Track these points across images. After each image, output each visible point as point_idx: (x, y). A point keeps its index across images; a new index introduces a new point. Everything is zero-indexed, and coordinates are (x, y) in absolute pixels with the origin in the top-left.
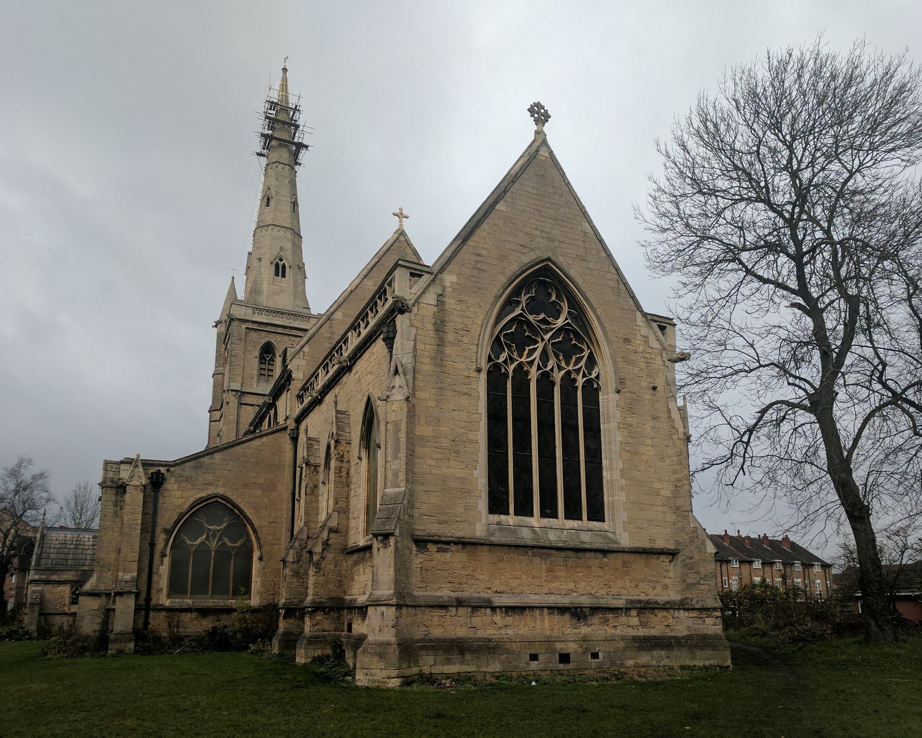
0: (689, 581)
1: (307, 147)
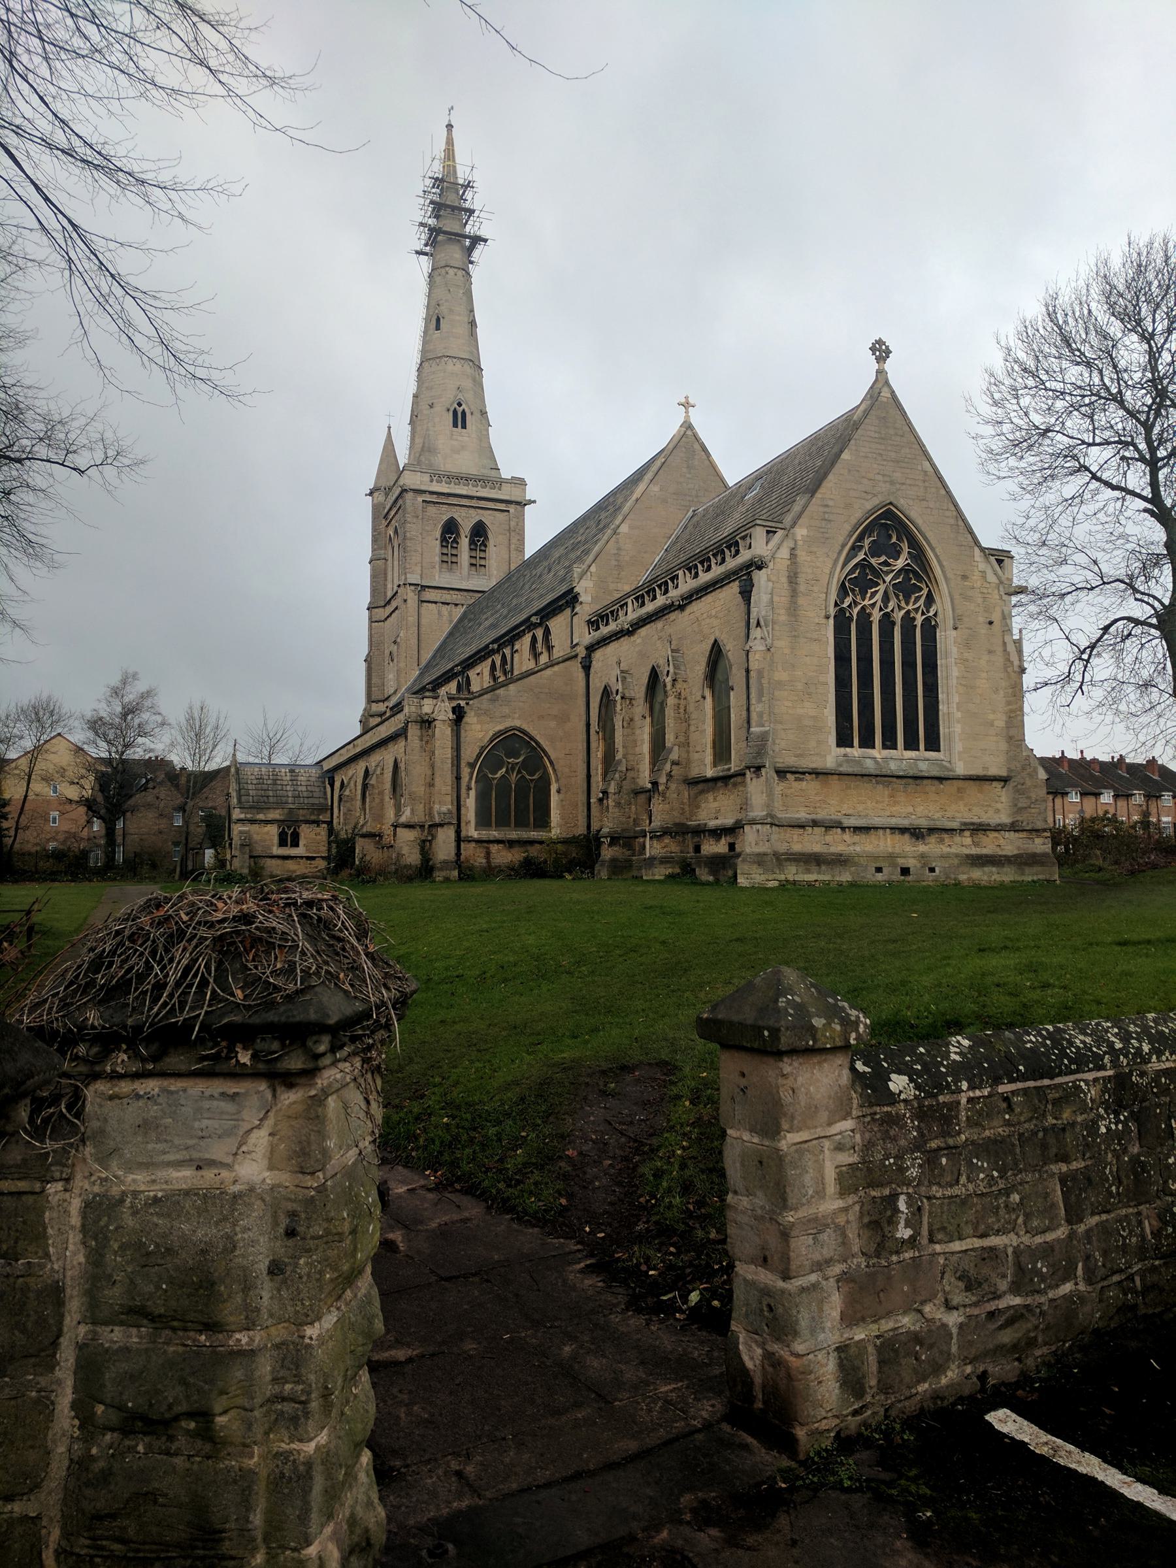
0: (1020, 805)
1: (486, 241)
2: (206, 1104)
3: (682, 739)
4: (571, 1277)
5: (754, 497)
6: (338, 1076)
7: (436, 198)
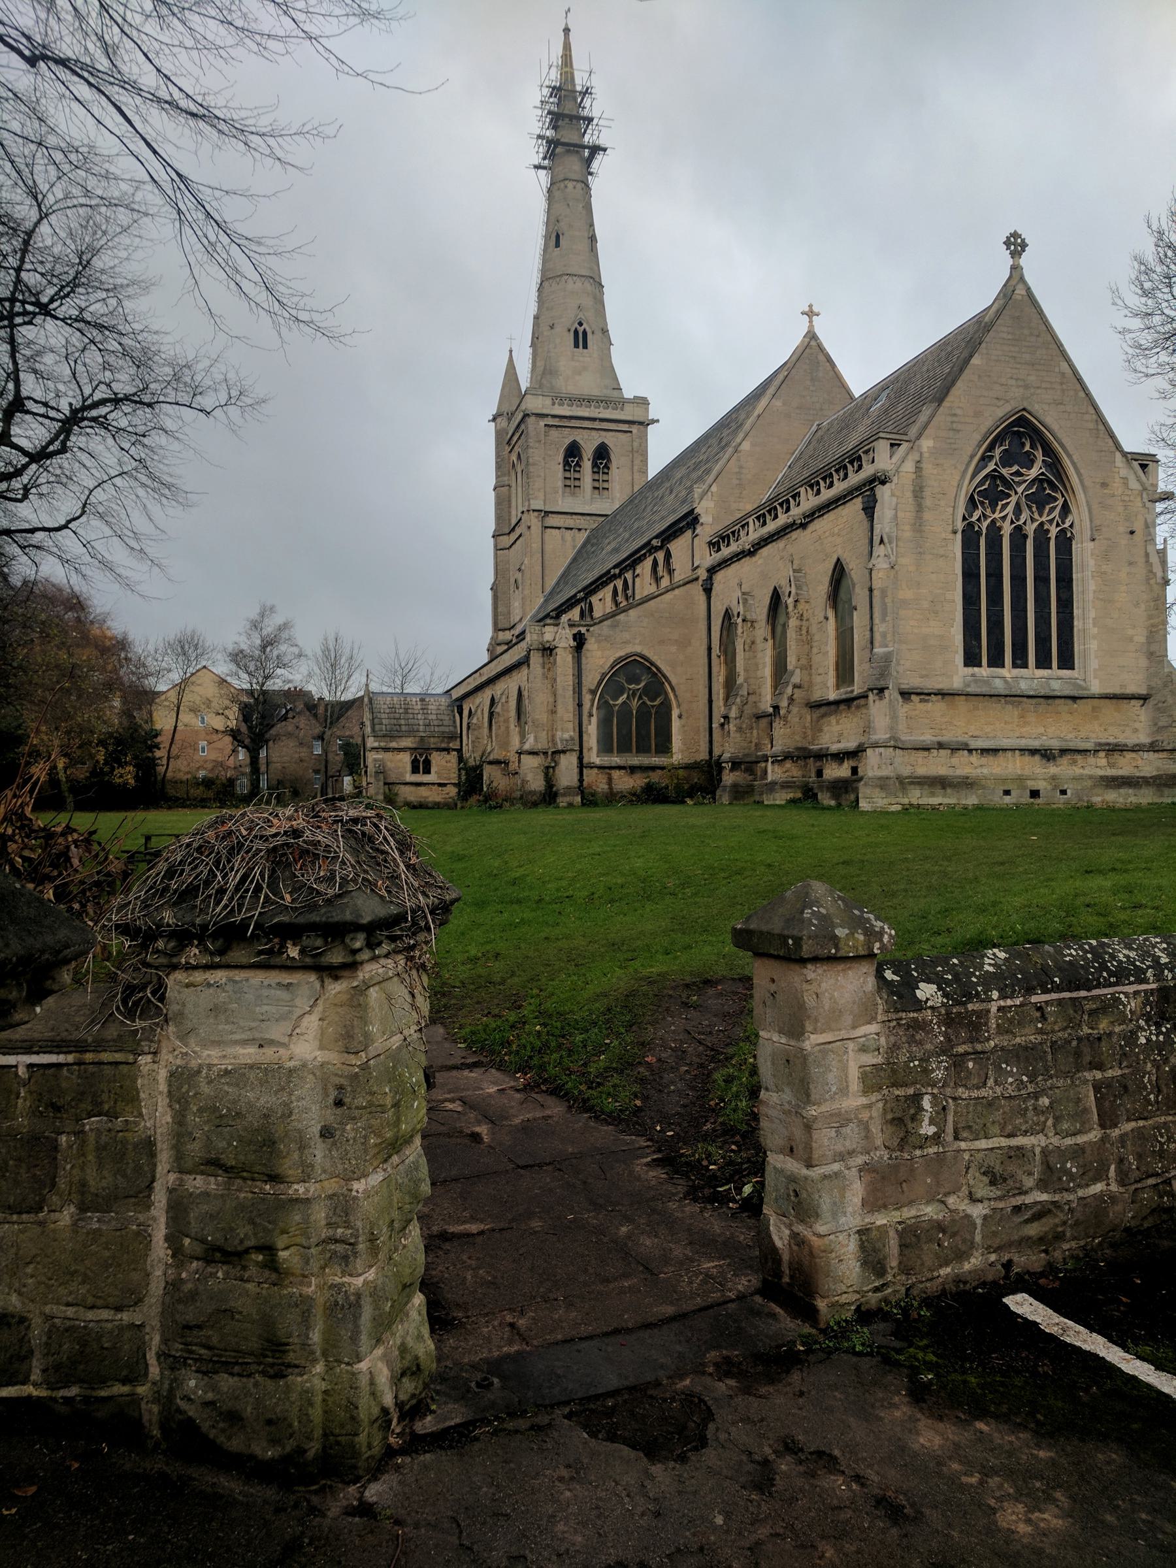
0: (1160, 724)
1: (605, 150)
2: (265, 992)
3: (803, 661)
4: (638, 1169)
5: (880, 409)
6: (381, 971)
7: (554, 108)
